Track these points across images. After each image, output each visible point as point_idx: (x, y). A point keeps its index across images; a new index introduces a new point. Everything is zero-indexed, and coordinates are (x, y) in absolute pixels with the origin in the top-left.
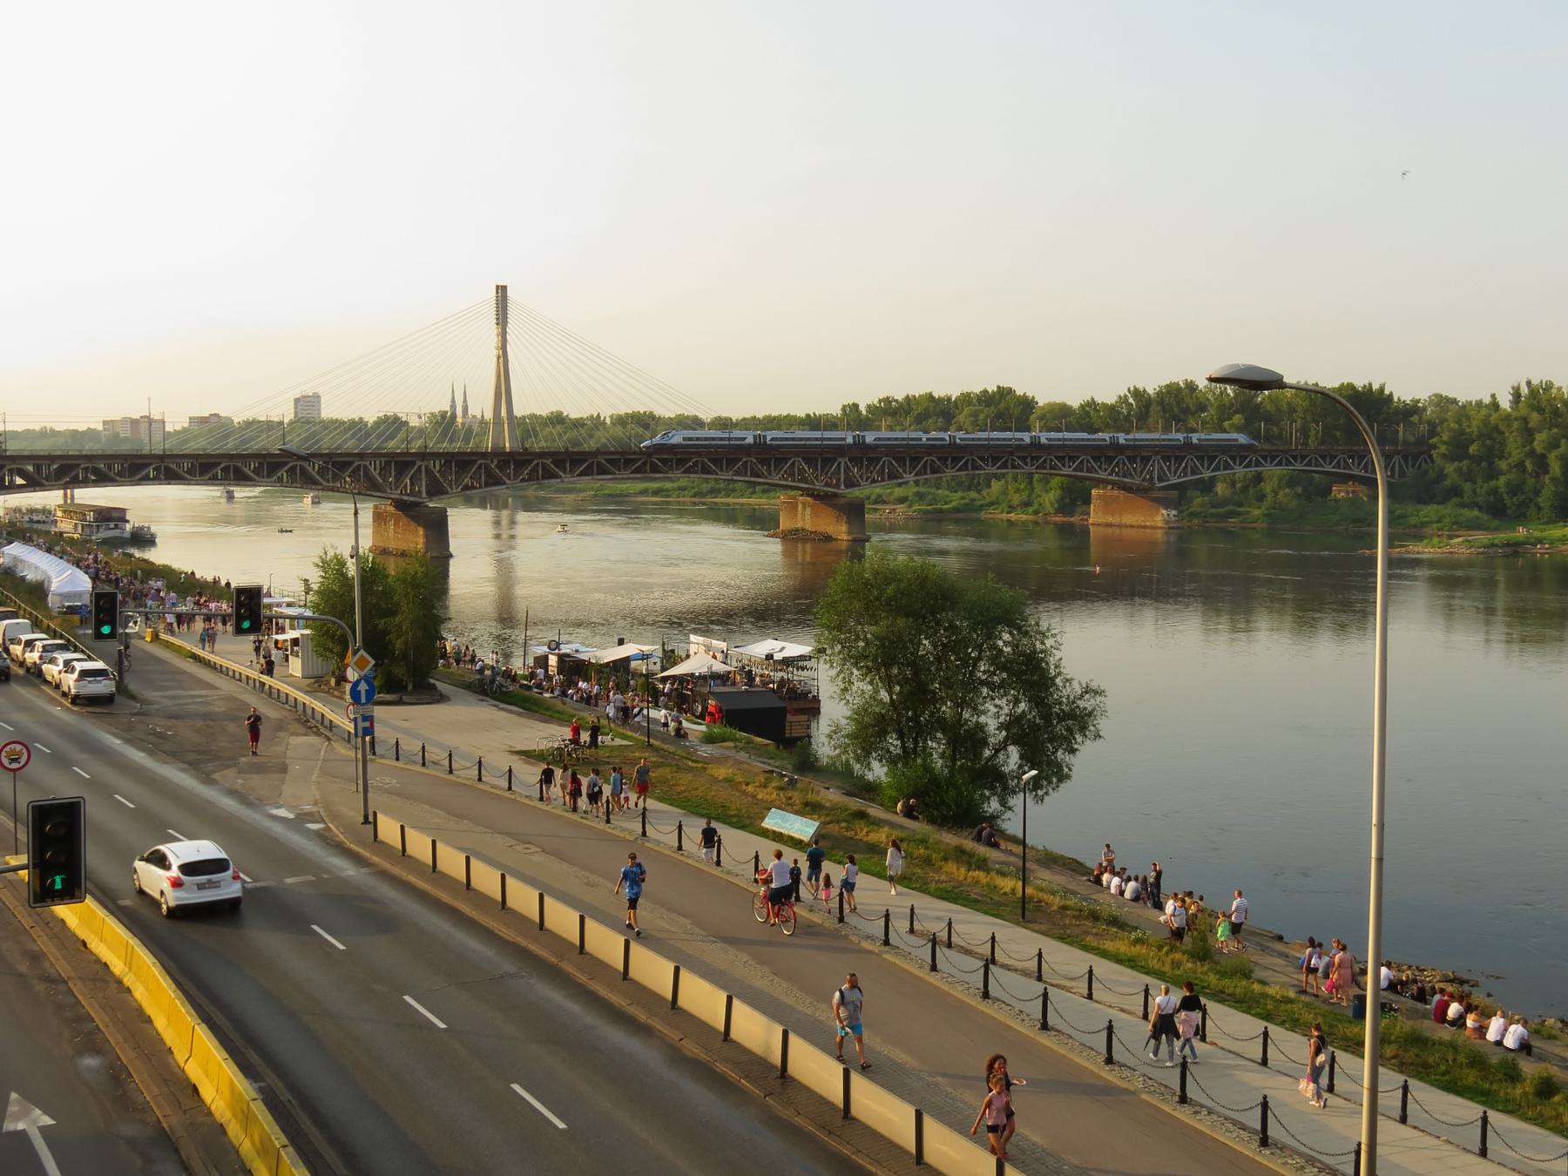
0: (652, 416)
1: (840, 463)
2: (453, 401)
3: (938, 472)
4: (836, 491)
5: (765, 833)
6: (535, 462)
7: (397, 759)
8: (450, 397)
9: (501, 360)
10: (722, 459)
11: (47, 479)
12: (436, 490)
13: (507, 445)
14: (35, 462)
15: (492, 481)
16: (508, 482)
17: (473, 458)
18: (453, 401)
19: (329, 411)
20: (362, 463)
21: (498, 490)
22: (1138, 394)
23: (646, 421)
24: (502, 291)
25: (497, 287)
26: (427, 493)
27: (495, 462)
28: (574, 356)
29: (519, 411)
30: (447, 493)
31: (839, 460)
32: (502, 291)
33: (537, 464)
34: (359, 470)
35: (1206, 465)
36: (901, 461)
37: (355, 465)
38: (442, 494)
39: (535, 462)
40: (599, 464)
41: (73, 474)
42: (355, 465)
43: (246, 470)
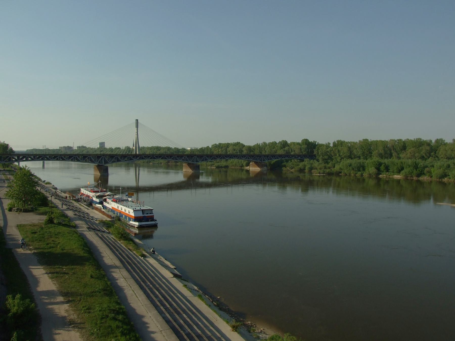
0: (160, 147)
1: (103, 157)
2: (134, 143)
3: (207, 160)
4: (194, 163)
5: (109, 231)
6: (128, 157)
7: (118, 206)
8: (133, 144)
9: (137, 135)
10: (190, 156)
11: (52, 159)
12: (106, 162)
13: (138, 153)
14: (18, 156)
15: (118, 161)
16: (122, 161)
17: (114, 156)
18: (134, 143)
19: (107, 146)
20: (116, 156)
21: (119, 163)
22: (265, 143)
23: (158, 148)
24: (137, 120)
25: (136, 120)
26: (104, 163)
27: (132, 156)
28: (156, 135)
29: (141, 146)
30: (109, 163)
31: (194, 156)
32: (137, 120)
33: (129, 157)
34: (89, 158)
35: (305, 157)
36: (272, 156)
37: (88, 157)
38: (107, 163)
39: (128, 157)
40: (154, 157)
41: (57, 158)
42: (88, 157)
43: (79, 159)
